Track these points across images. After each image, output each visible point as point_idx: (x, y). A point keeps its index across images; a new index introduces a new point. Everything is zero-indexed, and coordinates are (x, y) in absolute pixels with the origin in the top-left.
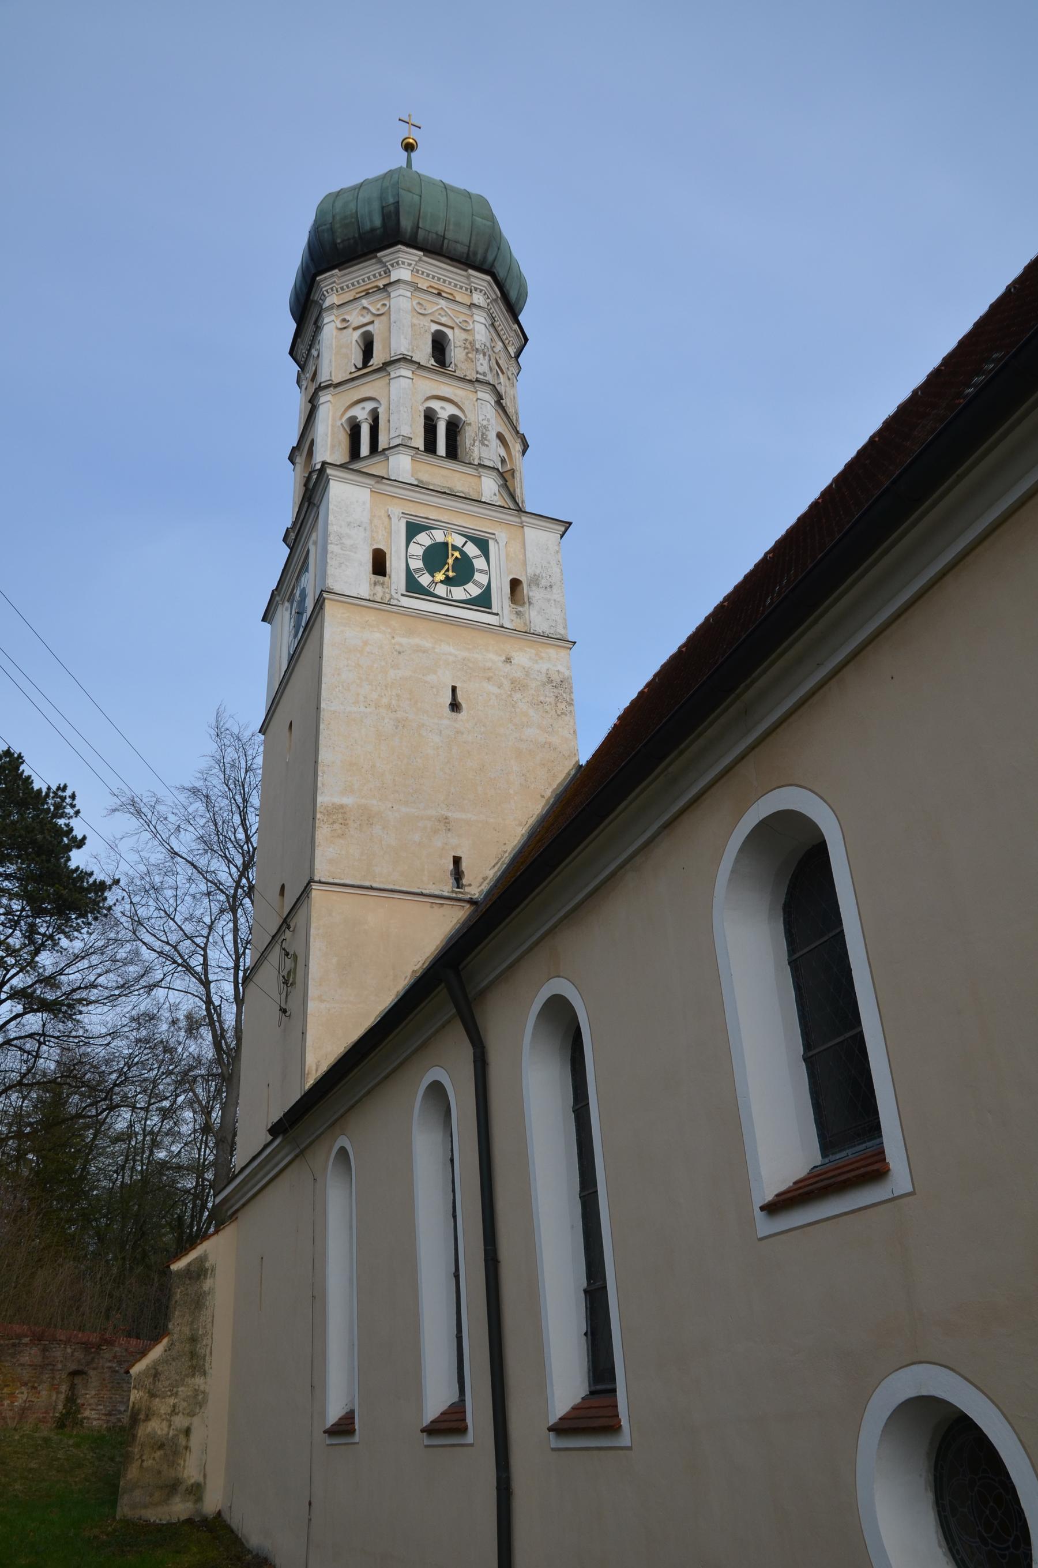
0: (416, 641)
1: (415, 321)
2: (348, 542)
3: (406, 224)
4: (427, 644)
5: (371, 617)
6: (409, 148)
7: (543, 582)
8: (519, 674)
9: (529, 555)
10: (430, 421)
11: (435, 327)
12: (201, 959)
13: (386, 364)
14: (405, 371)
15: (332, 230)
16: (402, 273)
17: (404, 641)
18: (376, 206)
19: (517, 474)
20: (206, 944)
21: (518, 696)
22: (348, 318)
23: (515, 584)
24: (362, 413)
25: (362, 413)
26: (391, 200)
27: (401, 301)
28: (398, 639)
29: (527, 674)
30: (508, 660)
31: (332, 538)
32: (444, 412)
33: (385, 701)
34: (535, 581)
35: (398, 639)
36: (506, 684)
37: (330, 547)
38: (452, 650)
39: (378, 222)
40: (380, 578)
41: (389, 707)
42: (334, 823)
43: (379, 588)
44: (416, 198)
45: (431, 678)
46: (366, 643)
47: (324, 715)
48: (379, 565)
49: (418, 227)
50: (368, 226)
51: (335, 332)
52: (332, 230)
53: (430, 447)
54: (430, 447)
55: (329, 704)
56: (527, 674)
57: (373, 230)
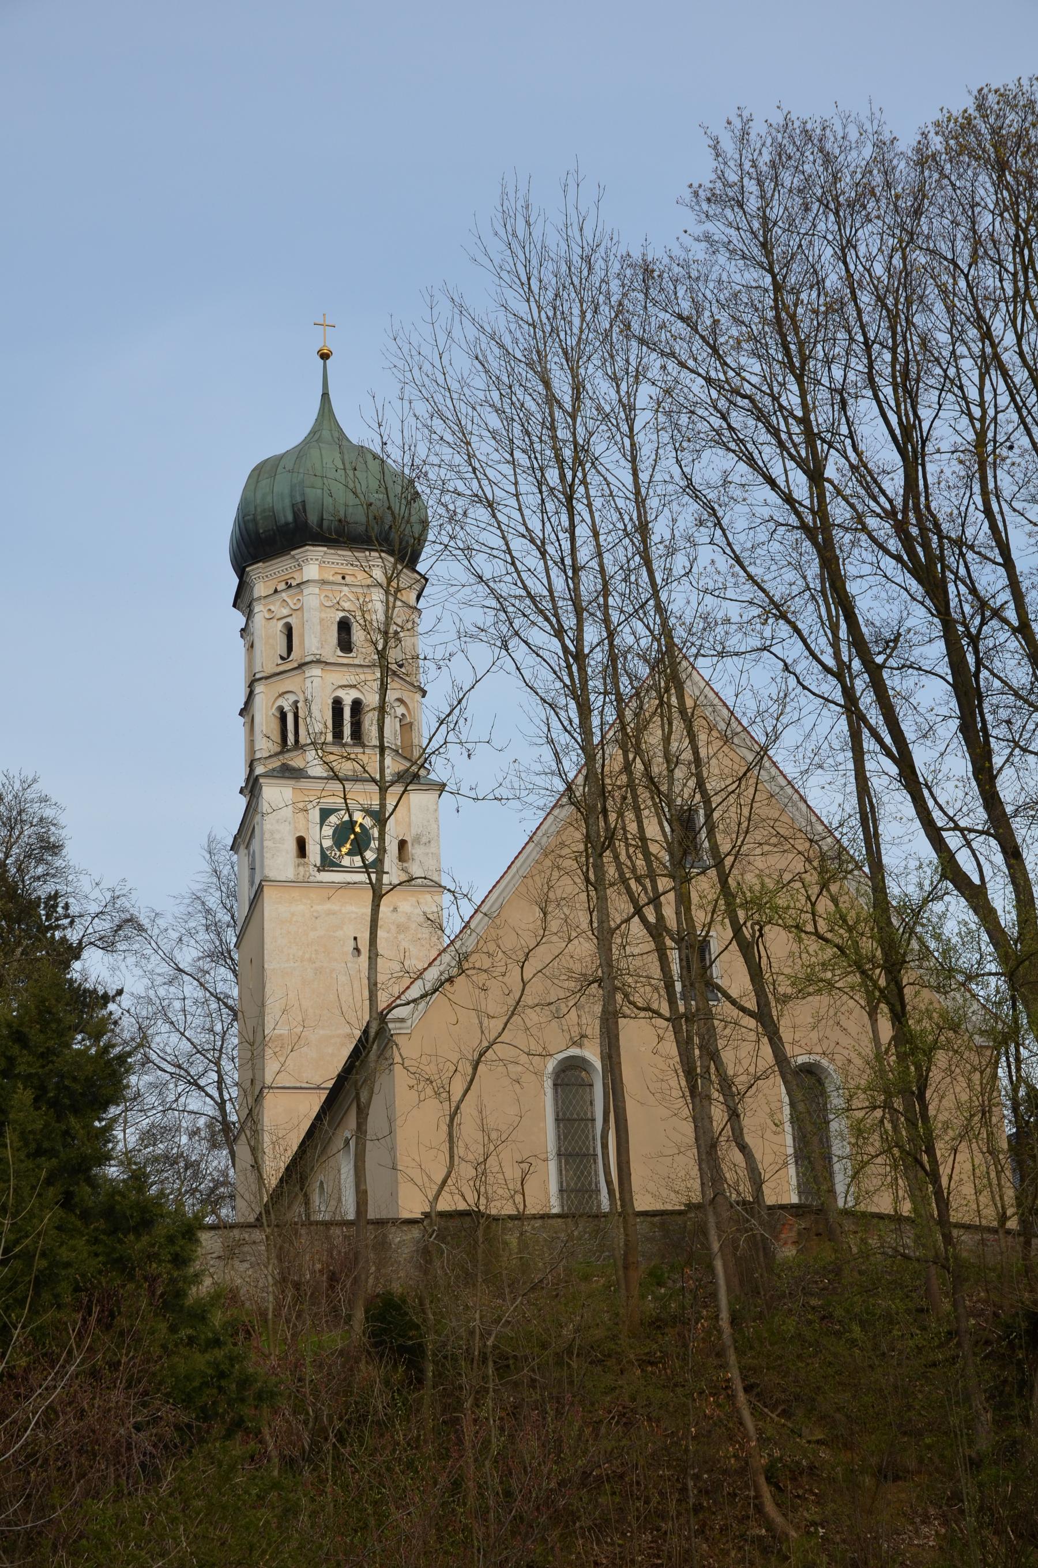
0: (328, 906)
1: (324, 615)
2: (277, 836)
3: (313, 519)
4: (335, 907)
5: (296, 894)
6: (325, 357)
7: (424, 840)
8: (402, 919)
9: (413, 818)
10: (337, 706)
11: (341, 614)
12: (215, 1076)
13: (301, 666)
14: (315, 671)
15: (254, 520)
16: (311, 571)
17: (319, 908)
18: (287, 502)
19: (415, 727)
20: (219, 1058)
21: (401, 937)
22: (273, 608)
23: (402, 844)
24: (287, 704)
25: (287, 704)
26: (299, 499)
27: (312, 597)
28: (315, 907)
29: (409, 918)
30: (395, 910)
31: (267, 836)
32: (348, 698)
33: (307, 956)
34: (417, 840)
35: (315, 907)
36: (393, 928)
37: (266, 843)
38: (354, 909)
39: (290, 518)
40: (302, 860)
41: (310, 960)
42: (780, 1358)
43: (301, 869)
44: (319, 491)
45: (339, 933)
46: (293, 914)
47: (268, 973)
48: (301, 844)
49: (322, 519)
50: (282, 521)
51: (263, 621)
52: (254, 520)
53: (338, 734)
54: (338, 734)
55: (271, 964)
56: (409, 918)
57: (287, 524)
